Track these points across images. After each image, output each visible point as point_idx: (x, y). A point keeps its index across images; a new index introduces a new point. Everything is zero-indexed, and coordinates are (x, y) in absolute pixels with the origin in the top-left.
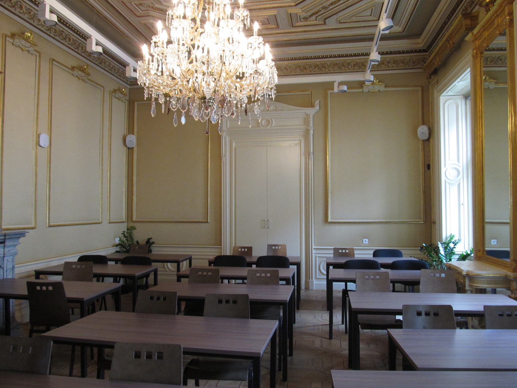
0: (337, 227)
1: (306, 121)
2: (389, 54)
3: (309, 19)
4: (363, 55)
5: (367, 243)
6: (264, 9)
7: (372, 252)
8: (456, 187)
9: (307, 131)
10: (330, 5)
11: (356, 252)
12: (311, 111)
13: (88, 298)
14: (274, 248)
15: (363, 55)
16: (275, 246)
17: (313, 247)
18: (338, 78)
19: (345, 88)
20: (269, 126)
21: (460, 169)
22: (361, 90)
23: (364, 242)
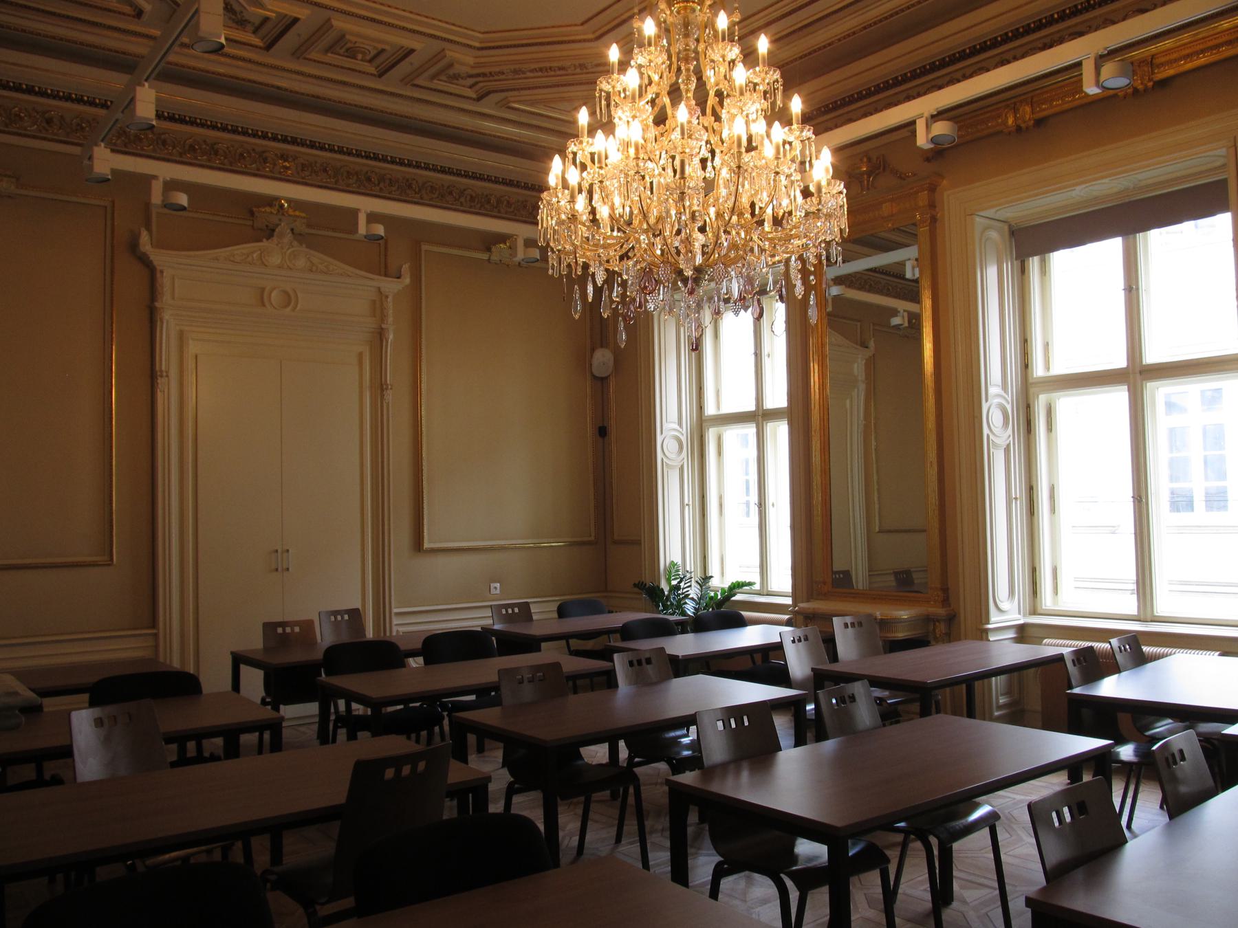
0: (441, 560)
1: (378, 307)
2: (289, 143)
3: (461, 82)
4: (526, 187)
5: (498, 591)
6: (414, 31)
7: (554, 607)
8: (677, 472)
9: (380, 334)
10: (532, 71)
11: (915, 576)
12: (391, 287)
13: (345, 794)
14: (280, 630)
15: (526, 187)
16: (283, 624)
17: (395, 610)
18: (365, 204)
19: (183, 199)
20: (288, 309)
21: (683, 439)
22: (485, 256)
23: (493, 591)
